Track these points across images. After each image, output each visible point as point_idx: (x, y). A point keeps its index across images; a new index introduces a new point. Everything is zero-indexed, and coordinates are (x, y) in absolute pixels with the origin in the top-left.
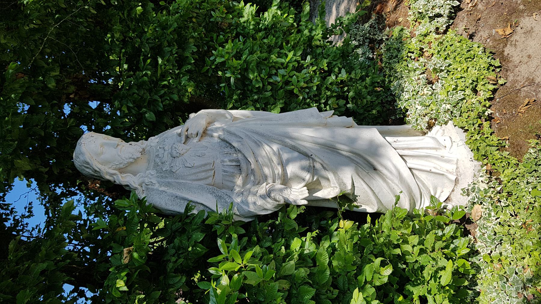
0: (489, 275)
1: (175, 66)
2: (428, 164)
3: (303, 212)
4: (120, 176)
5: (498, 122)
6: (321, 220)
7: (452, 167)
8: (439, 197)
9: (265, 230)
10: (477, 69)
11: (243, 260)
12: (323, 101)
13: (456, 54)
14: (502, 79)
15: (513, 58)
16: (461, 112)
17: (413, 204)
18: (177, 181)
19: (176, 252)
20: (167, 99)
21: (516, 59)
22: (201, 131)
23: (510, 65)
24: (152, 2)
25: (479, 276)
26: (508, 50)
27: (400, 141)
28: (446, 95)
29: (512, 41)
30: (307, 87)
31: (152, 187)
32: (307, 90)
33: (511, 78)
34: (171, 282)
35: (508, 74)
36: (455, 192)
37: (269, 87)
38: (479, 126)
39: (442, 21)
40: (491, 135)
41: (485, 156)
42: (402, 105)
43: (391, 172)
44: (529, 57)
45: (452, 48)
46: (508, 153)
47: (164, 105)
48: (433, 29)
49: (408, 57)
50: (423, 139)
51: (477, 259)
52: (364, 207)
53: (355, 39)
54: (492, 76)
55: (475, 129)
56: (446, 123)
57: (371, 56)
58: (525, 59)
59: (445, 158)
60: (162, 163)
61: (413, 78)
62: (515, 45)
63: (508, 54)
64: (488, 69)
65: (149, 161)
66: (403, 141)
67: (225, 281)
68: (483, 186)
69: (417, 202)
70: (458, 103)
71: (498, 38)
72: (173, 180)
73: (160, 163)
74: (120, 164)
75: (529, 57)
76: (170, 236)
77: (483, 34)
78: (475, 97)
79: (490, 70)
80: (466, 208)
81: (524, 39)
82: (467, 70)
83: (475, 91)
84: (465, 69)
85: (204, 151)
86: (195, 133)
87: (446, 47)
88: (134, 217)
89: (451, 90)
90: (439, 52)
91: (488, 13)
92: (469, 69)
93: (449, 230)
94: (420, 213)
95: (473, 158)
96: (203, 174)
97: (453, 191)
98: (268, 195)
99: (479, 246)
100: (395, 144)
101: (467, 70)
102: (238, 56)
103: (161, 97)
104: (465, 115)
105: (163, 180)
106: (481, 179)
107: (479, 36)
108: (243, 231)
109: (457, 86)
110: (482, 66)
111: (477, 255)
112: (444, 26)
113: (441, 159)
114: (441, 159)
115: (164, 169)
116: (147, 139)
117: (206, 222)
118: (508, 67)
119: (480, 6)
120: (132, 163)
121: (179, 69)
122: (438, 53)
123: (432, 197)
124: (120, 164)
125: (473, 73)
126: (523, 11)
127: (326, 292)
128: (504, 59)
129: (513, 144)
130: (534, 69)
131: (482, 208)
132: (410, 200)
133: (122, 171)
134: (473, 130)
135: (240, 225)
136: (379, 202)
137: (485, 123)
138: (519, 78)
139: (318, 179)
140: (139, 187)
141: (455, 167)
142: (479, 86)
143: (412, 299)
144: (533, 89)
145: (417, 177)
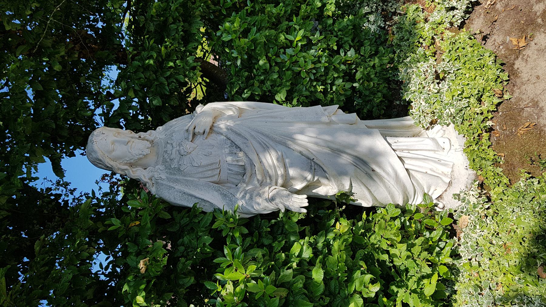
0: (466, 280)
1: (181, 44)
2: (424, 162)
3: (304, 217)
4: (131, 171)
5: (497, 135)
6: (319, 209)
7: (447, 170)
8: (432, 194)
9: (265, 231)
10: (485, 79)
11: (246, 271)
12: (329, 82)
13: (466, 59)
14: (508, 93)
15: (522, 74)
16: (463, 120)
17: (406, 200)
18: (185, 178)
19: (185, 250)
20: (174, 82)
21: (524, 76)
22: (208, 130)
23: (518, 81)
24: (195, 278)
25: (454, 297)
26: (519, 64)
27: (400, 142)
28: (451, 98)
29: (524, 55)
30: (314, 68)
31: (162, 182)
32: (314, 71)
33: (516, 95)
34: (181, 283)
35: (515, 89)
36: (447, 193)
37: (277, 69)
38: (479, 136)
39: (459, 13)
40: (488, 147)
41: (481, 169)
42: (407, 97)
43: (388, 174)
44: (538, 77)
45: (464, 52)
46: (501, 169)
47: (170, 89)
48: (447, 20)
49: (419, 43)
50: (423, 141)
51: (458, 262)
52: (359, 201)
53: (368, 5)
54: (498, 88)
55: (474, 138)
56: (448, 125)
57: (383, 26)
58: (534, 79)
59: (442, 162)
60: (171, 160)
61: (422, 70)
62: (527, 60)
63: (518, 68)
64: (496, 81)
65: (158, 154)
66: (402, 142)
67: (230, 287)
68: (473, 200)
69: (411, 198)
70: (462, 110)
71: (511, 48)
72: (181, 177)
73: (168, 160)
74: (131, 159)
75: (538, 77)
76: (179, 230)
77: (497, 38)
78: (478, 105)
79: (498, 82)
80: (455, 211)
81: (535, 57)
82: (475, 79)
83: (479, 100)
84: (473, 77)
85: (210, 150)
86: (202, 131)
87: (458, 48)
88: (147, 223)
89: (457, 95)
90: (450, 51)
91: (506, 16)
92: (477, 78)
93: (436, 235)
94: (412, 209)
95: (468, 167)
96: (210, 172)
97: (446, 191)
98: (272, 199)
99: (462, 251)
100: (395, 144)
101: (475, 79)
102: (245, 33)
103: (167, 78)
104: (467, 123)
105: (172, 176)
106: (471, 193)
107: (493, 39)
108: (246, 231)
109: (463, 92)
110: (490, 78)
111: (458, 259)
112: (459, 21)
113: (439, 161)
114: (439, 161)
115: (173, 167)
116: (155, 130)
117: (214, 227)
118: (516, 83)
119: (498, 6)
120: (141, 158)
121: (185, 46)
122: (449, 52)
123: (425, 195)
124: (131, 159)
125: (481, 82)
126: (540, 26)
127: (319, 300)
128: (513, 73)
129: (508, 162)
130: (540, 92)
131: (470, 219)
132: (404, 198)
133: (131, 165)
134: (472, 139)
135: (244, 223)
136: (374, 198)
137: (484, 134)
138: (524, 97)
139: (318, 179)
140: (149, 181)
141: (451, 170)
142: (484, 96)
143: (395, 301)
144: (536, 111)
145: (413, 177)
